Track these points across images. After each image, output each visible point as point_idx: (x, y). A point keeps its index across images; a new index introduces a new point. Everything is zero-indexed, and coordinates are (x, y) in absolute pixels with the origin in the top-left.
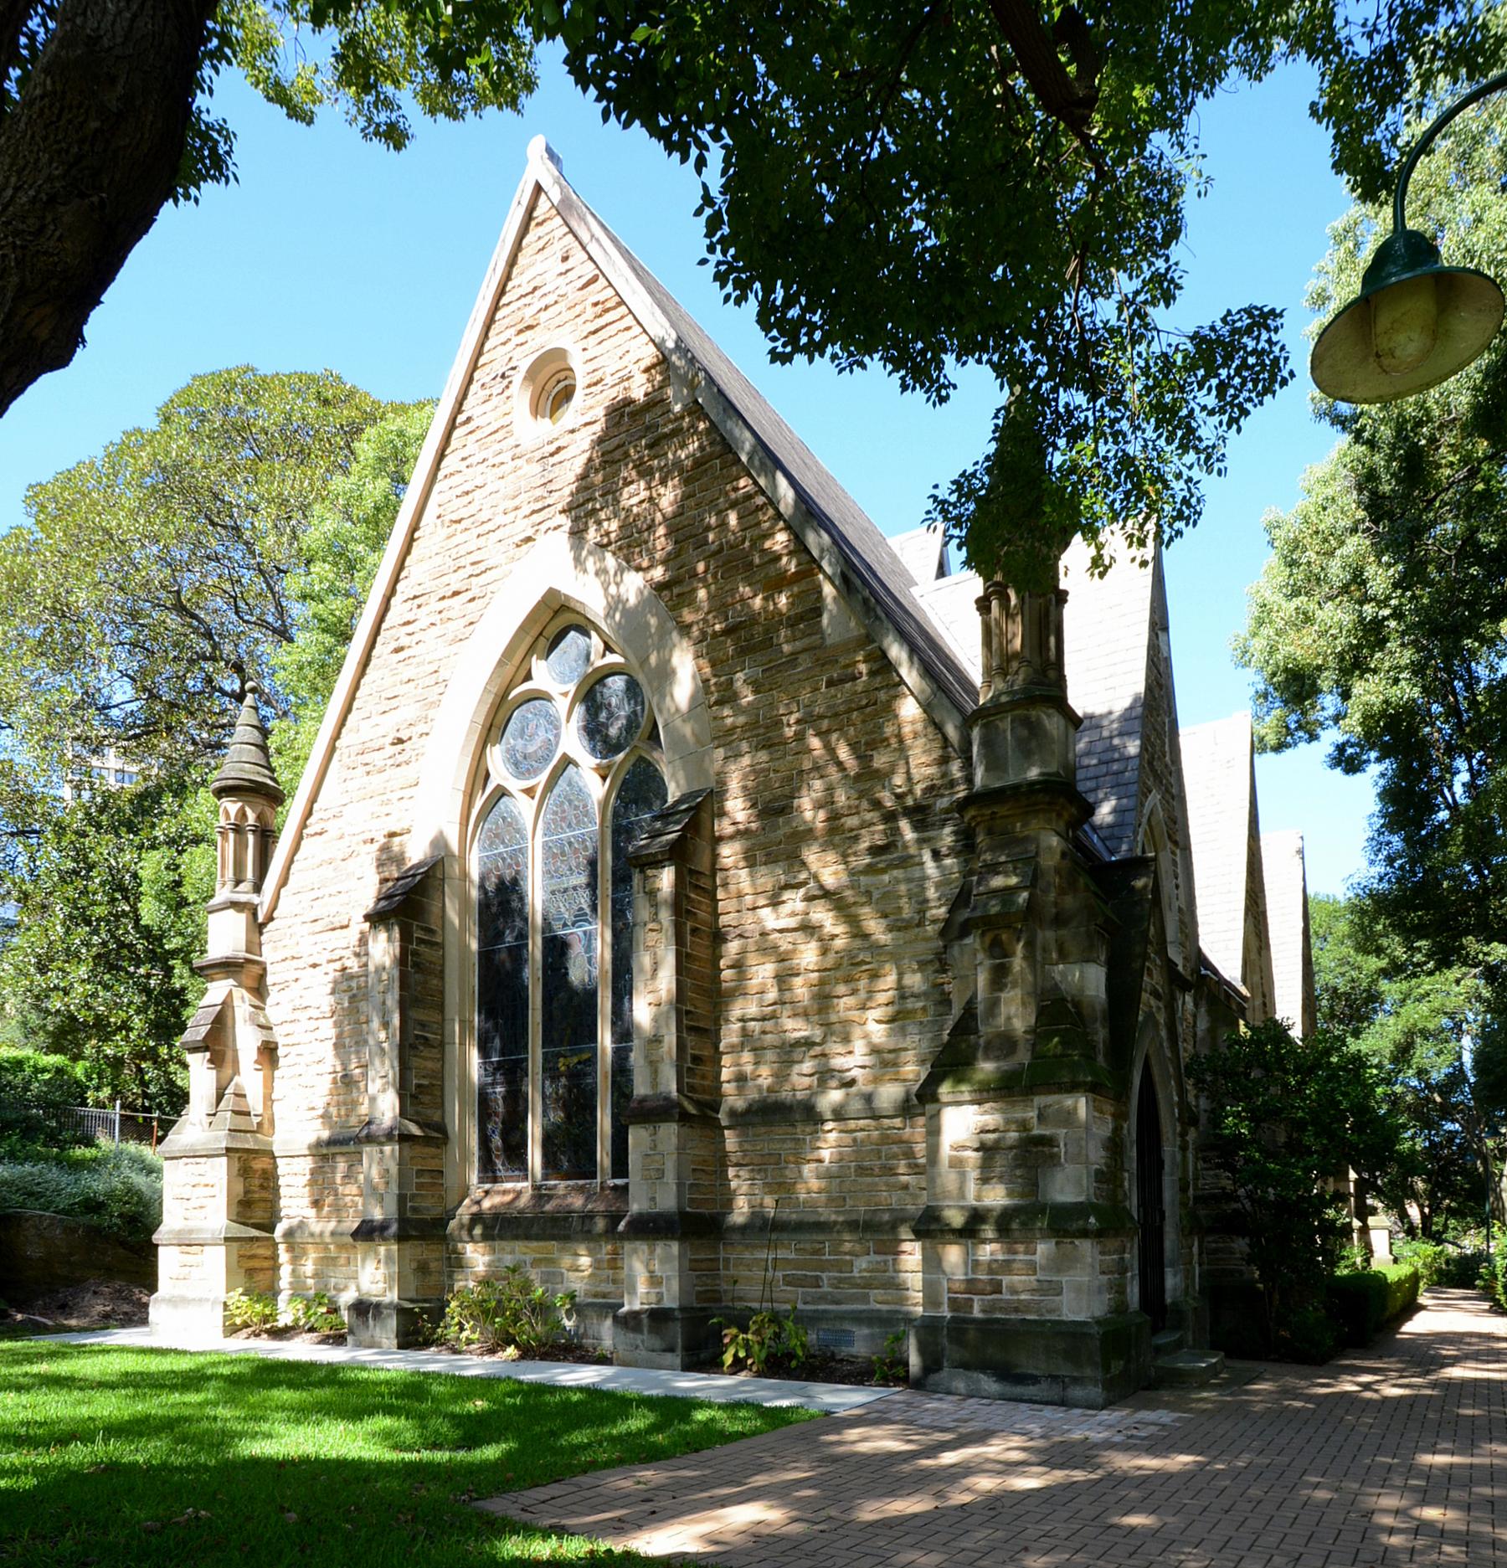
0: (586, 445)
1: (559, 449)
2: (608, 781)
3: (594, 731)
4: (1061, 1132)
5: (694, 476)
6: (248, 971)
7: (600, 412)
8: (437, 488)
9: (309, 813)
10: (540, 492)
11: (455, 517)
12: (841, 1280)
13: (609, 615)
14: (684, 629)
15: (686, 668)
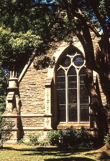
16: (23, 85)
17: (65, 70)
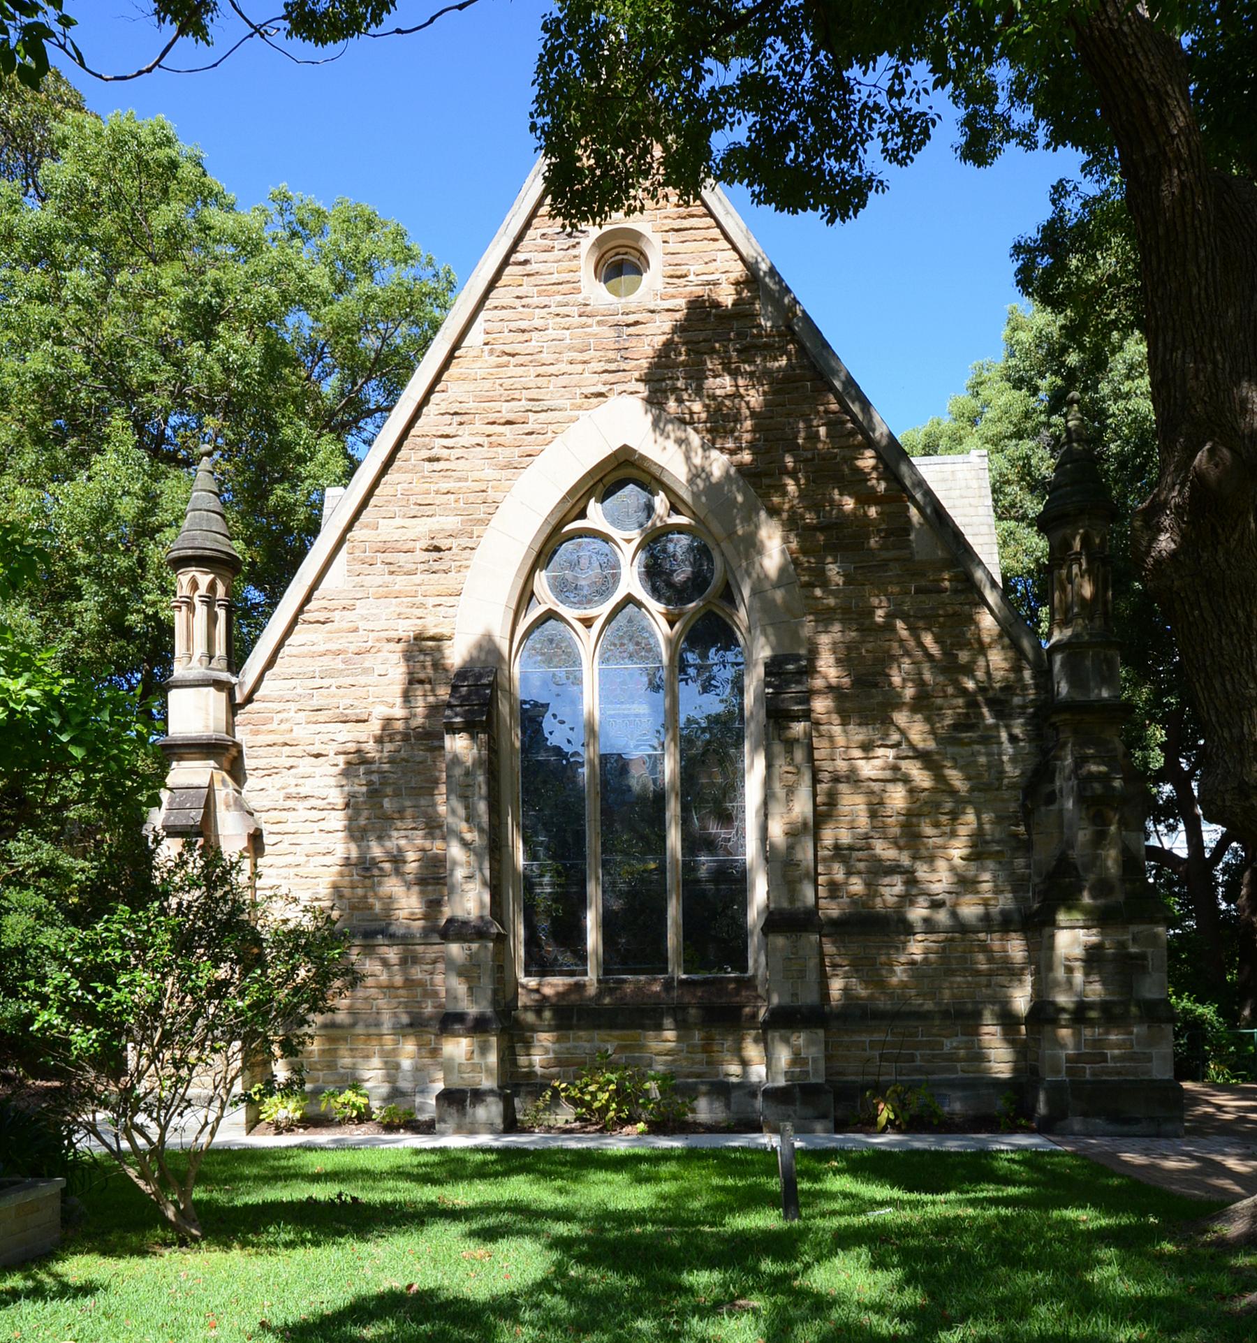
0: (667, 327)
1: (636, 323)
2: (677, 626)
3: (655, 574)
4: (1150, 950)
5: (780, 387)
6: (225, 753)
7: (681, 303)
8: (483, 315)
9: (308, 599)
10: (611, 355)
11: (508, 349)
12: (934, 1056)
13: (691, 481)
14: (773, 512)
15: (774, 547)
16: (274, 726)
17: (579, 626)
